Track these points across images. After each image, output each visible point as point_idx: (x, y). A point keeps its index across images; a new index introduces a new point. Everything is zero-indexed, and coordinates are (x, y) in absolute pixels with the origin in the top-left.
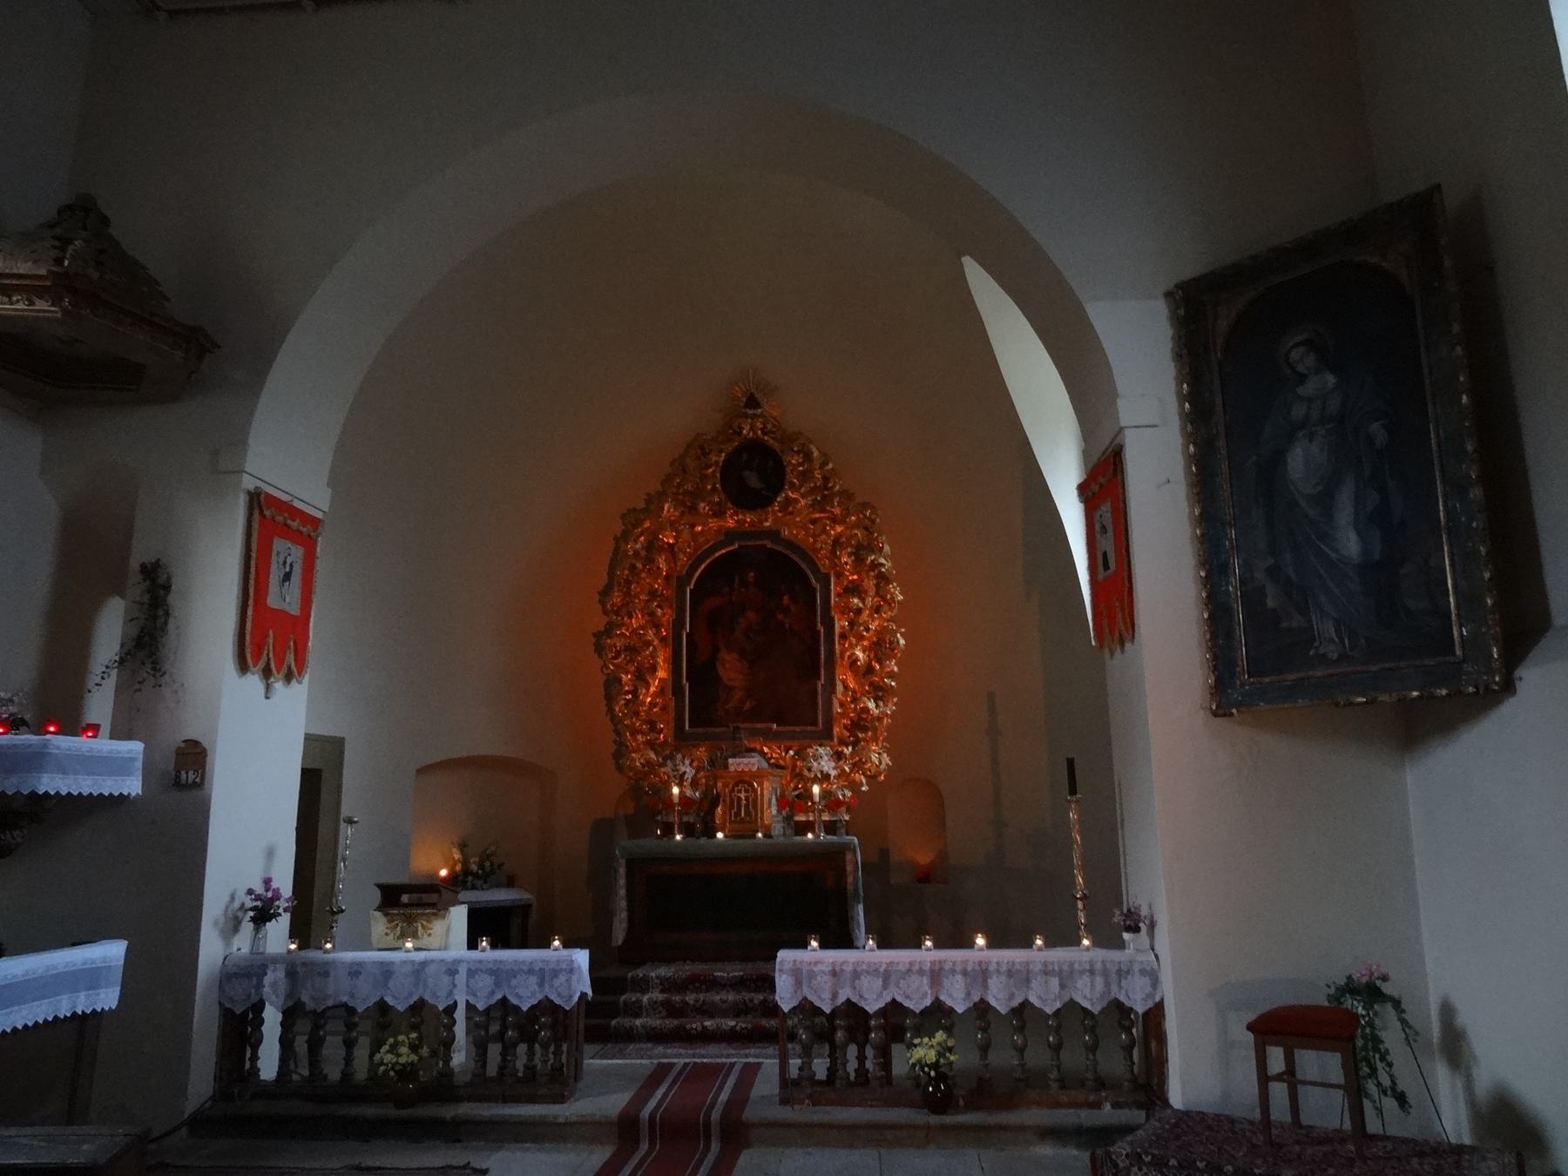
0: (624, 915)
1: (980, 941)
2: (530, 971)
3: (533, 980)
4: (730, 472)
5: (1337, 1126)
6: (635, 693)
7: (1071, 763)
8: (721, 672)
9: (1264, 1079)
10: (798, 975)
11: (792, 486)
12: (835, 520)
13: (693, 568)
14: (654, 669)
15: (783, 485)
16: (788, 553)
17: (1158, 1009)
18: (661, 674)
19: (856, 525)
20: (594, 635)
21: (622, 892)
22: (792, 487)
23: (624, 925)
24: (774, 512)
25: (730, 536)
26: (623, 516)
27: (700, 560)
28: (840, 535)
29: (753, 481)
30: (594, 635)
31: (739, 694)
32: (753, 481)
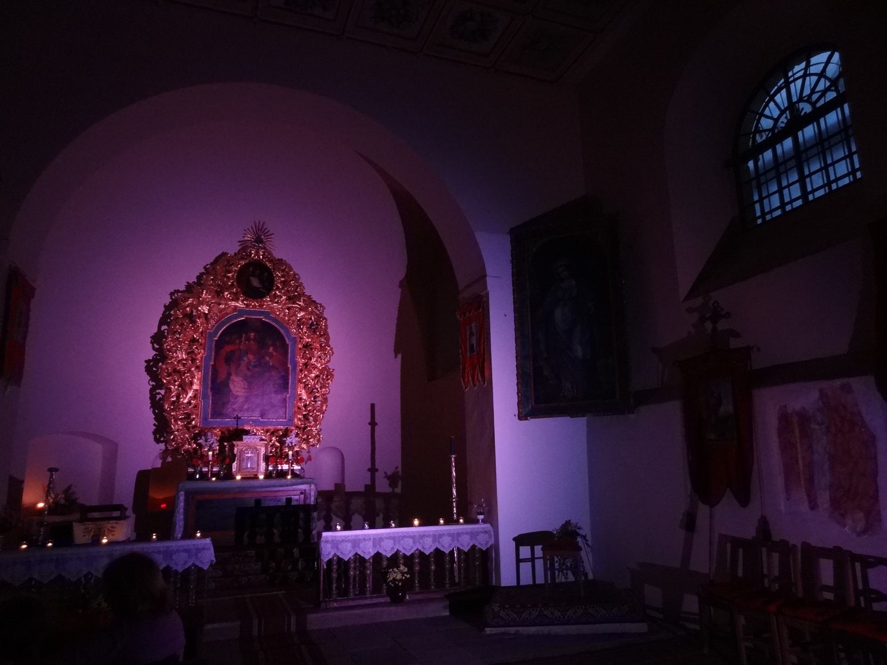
0: (182, 523)
1: (416, 522)
2: (389, 538)
3: (411, 540)
4: (243, 278)
5: (531, 583)
6: (178, 397)
7: (373, 406)
8: (231, 386)
9: (519, 561)
10: (335, 543)
11: (278, 288)
12: (301, 309)
13: (218, 328)
14: (191, 383)
15: (272, 287)
16: (274, 324)
17: (788, 489)
18: (195, 387)
19: (312, 313)
20: (146, 361)
21: (182, 511)
22: (278, 288)
23: (182, 529)
24: (267, 301)
25: (241, 312)
26: (172, 294)
27: (224, 324)
28: (302, 317)
29: (255, 283)
30: (146, 361)
31: (241, 400)
32: (255, 283)
